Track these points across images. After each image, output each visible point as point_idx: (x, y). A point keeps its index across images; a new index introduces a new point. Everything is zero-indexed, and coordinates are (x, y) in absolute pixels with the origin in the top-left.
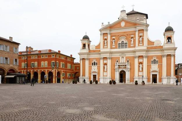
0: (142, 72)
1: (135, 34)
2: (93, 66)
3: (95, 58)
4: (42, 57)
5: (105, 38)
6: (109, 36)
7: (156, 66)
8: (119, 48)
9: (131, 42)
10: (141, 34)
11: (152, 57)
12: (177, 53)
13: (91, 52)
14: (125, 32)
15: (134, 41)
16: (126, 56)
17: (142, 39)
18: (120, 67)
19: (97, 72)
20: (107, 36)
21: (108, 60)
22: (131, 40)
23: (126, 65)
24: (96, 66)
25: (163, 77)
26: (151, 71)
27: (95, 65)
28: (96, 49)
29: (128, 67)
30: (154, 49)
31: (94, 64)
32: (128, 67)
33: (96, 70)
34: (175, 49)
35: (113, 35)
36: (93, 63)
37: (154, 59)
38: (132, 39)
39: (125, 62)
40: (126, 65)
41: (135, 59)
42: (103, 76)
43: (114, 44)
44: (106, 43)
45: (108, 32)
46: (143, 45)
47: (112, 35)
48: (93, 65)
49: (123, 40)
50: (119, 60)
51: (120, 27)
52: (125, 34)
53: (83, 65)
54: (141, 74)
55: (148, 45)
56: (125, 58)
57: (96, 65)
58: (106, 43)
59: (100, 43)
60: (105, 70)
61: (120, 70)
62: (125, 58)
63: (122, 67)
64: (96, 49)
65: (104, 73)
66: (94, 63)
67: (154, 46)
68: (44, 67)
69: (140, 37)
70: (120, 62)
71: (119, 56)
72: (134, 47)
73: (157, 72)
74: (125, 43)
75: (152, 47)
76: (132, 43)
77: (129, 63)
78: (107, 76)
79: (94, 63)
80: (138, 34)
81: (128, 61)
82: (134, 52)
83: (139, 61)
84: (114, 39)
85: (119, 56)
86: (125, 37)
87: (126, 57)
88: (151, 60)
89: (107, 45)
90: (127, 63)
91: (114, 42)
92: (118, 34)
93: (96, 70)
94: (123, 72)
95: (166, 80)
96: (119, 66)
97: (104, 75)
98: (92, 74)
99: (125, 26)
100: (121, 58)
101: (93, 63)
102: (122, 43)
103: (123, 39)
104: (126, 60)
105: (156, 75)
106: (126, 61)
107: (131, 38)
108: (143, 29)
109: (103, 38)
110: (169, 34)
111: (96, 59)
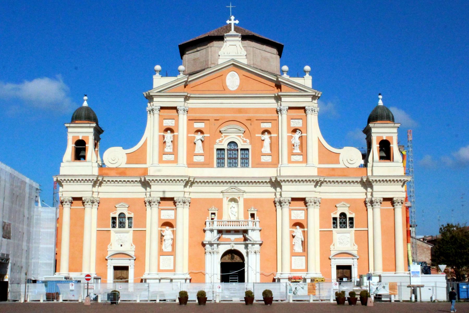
0: (304, 258)
1: (277, 120)
2: (117, 229)
3: (347, 201)
5: (168, 123)
6: (183, 118)
7: (348, 235)
8: (221, 164)
9: (262, 146)
10: (297, 124)
11: (334, 203)
13: (107, 175)
14: (240, 111)
15: (275, 145)
16: (246, 196)
17: (301, 138)
18: (225, 236)
19: (132, 254)
20: (176, 119)
21: (88, 208)
23: (245, 231)
24: (127, 232)
25: (117, 285)
26: (333, 253)
27: (122, 225)
28: (127, 163)
30: (339, 176)
31: (120, 223)
32: (254, 236)
33: (129, 248)
35: (197, 116)
37: (340, 211)
38: (266, 137)
39: (242, 218)
40: (245, 232)
42: (159, 270)
43: (199, 148)
44: (169, 143)
45: (178, 102)
46: (305, 160)
48: (114, 227)
49: (233, 137)
50: (220, 209)
51: (225, 88)
52: (238, 116)
54: (166, 262)
55: (320, 162)
56: (241, 202)
57: (127, 228)
58: (169, 143)
60: (167, 247)
61: (223, 249)
62: (241, 202)
63: (233, 237)
64: (127, 163)
66: (122, 215)
67: (341, 166)
69: (295, 131)
70: (225, 218)
71: (220, 196)
72: (275, 164)
74: (240, 147)
75: (333, 169)
76: (266, 149)
77: (258, 223)
78: (174, 270)
79: (343, 215)
80: (289, 124)
81: (253, 215)
82: (276, 184)
83: (293, 218)
84: (200, 131)
85: (220, 196)
86: (243, 129)
87: (246, 201)
88: (112, 215)
89: (175, 152)
90: (251, 224)
91: (199, 143)
92: (217, 116)
93: (129, 248)
96: (220, 232)
97: (161, 268)
98: (112, 263)
99: (241, 88)
100: (225, 202)
101: (114, 218)
102: (233, 147)
103: (233, 135)
104: (246, 210)
106: (246, 217)
107: (263, 133)
109: (161, 123)
111: (130, 203)
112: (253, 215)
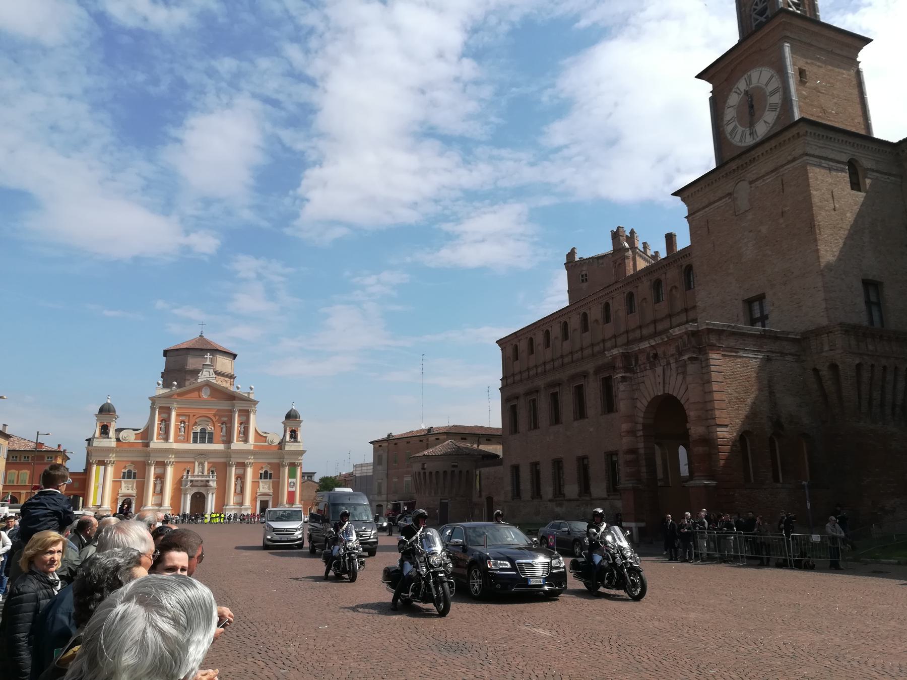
4: (46, 459)
8: (195, 441)
17: (244, 427)
22: (222, 428)
29: (213, 484)
34: (302, 453)
36: (261, 474)
41: (228, 468)
47: (265, 439)
53: (285, 476)
59: (149, 426)
61: (195, 490)
65: (100, 504)
68: (15, 484)
73: (270, 495)
94: (198, 496)
95: (674, 364)
101: (261, 474)
105: (267, 502)
108: (247, 408)
110: (292, 424)
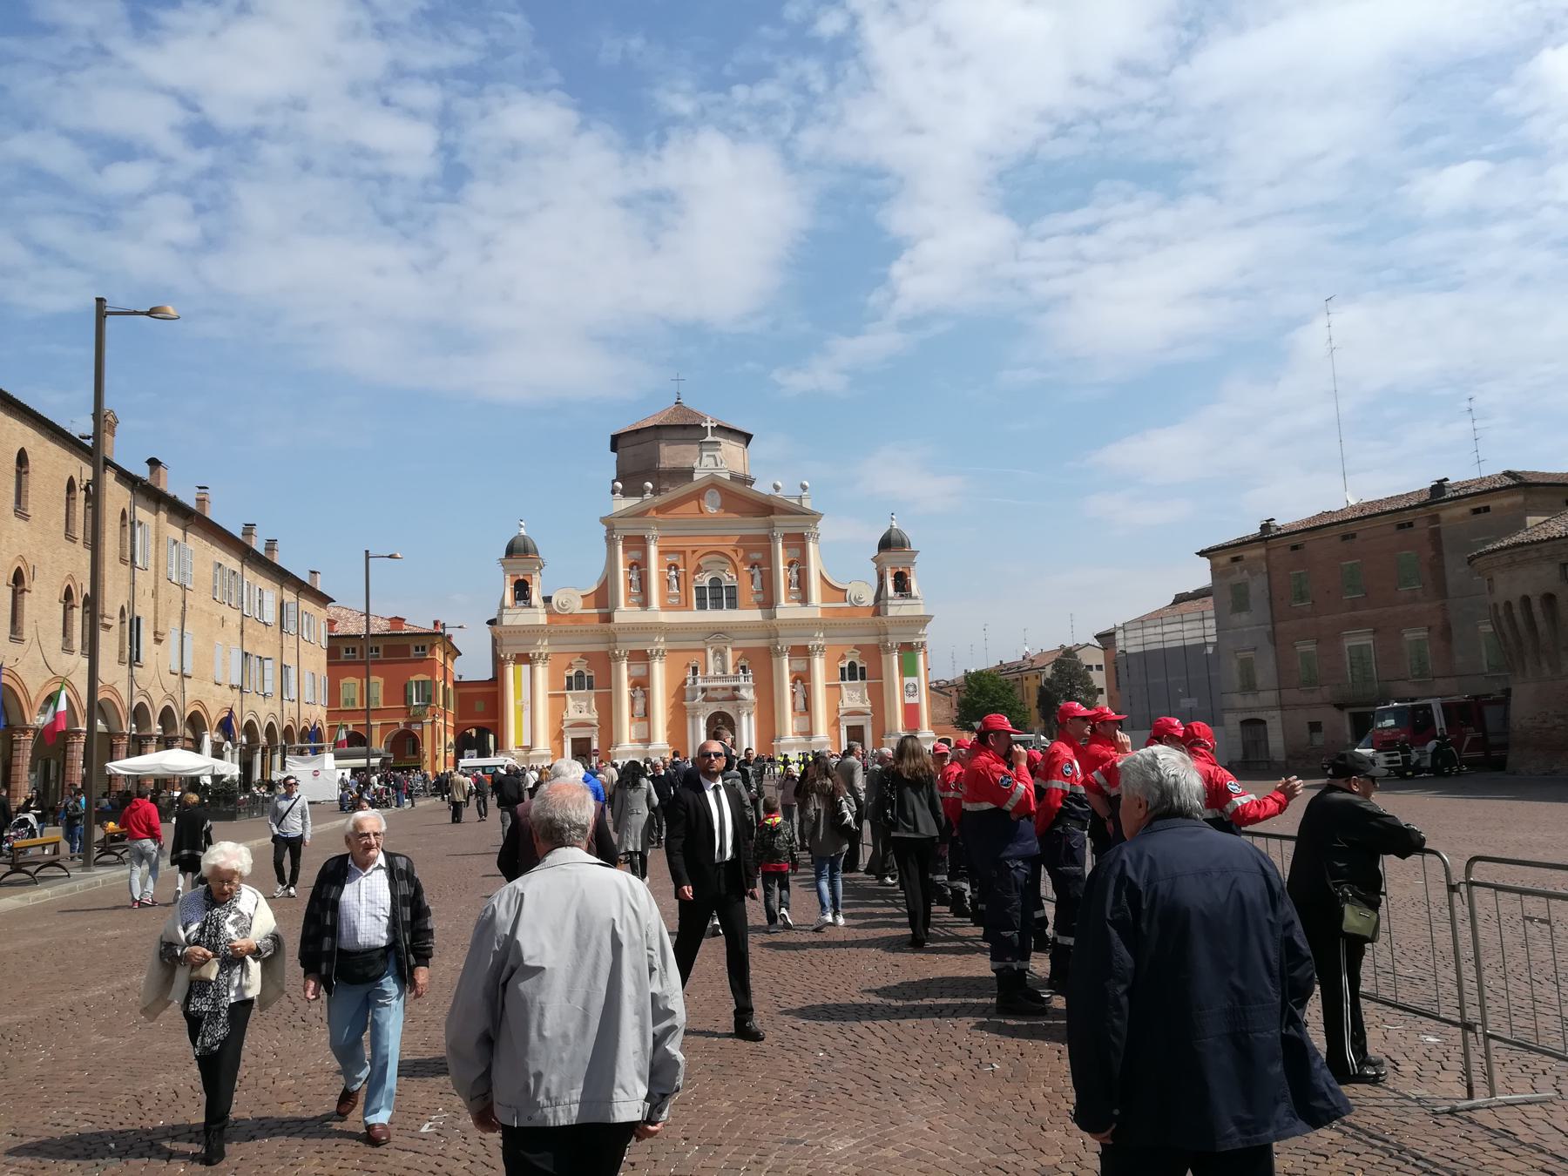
12: (930, 636)
27: (853, 677)
29: (748, 694)
34: (923, 621)
61: (713, 708)
112: (743, 668)
